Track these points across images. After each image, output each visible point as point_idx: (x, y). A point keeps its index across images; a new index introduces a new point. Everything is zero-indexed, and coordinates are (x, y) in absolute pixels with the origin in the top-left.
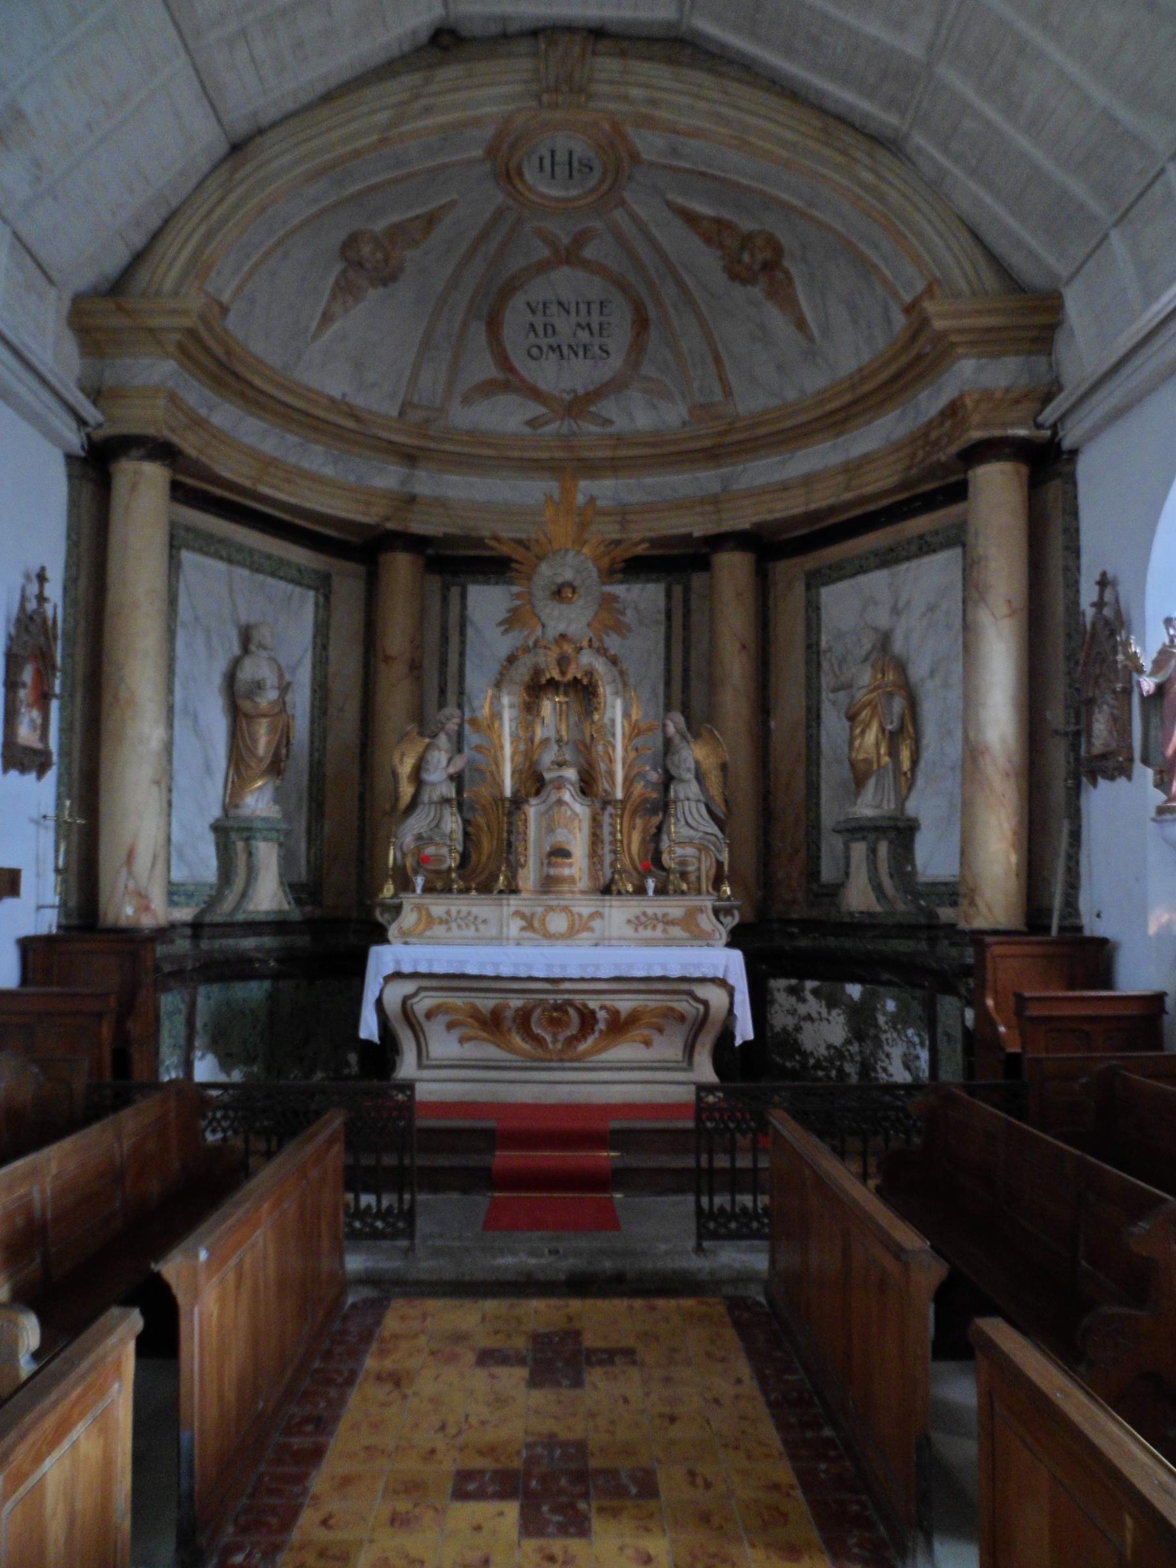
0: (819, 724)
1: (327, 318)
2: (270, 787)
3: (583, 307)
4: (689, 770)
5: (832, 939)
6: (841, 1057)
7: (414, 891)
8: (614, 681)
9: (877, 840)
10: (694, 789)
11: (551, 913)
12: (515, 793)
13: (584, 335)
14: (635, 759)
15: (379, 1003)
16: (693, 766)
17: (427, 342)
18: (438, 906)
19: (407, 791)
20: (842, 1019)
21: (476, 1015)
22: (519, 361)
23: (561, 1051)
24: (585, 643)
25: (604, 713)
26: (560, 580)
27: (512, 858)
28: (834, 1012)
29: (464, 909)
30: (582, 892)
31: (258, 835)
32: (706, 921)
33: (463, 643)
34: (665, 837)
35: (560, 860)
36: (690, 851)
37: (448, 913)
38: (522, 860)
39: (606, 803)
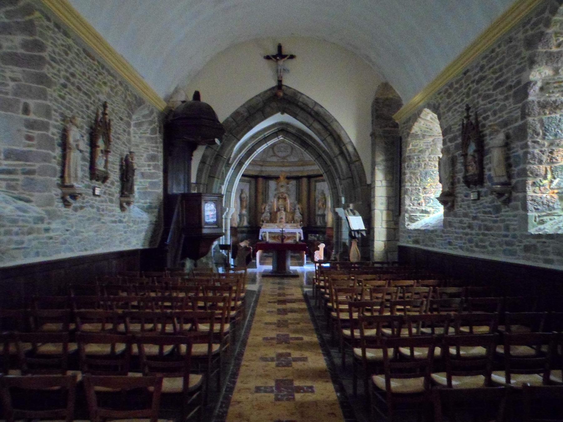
18: (267, 224)
19: (263, 211)
22: (276, 152)
32: (299, 226)
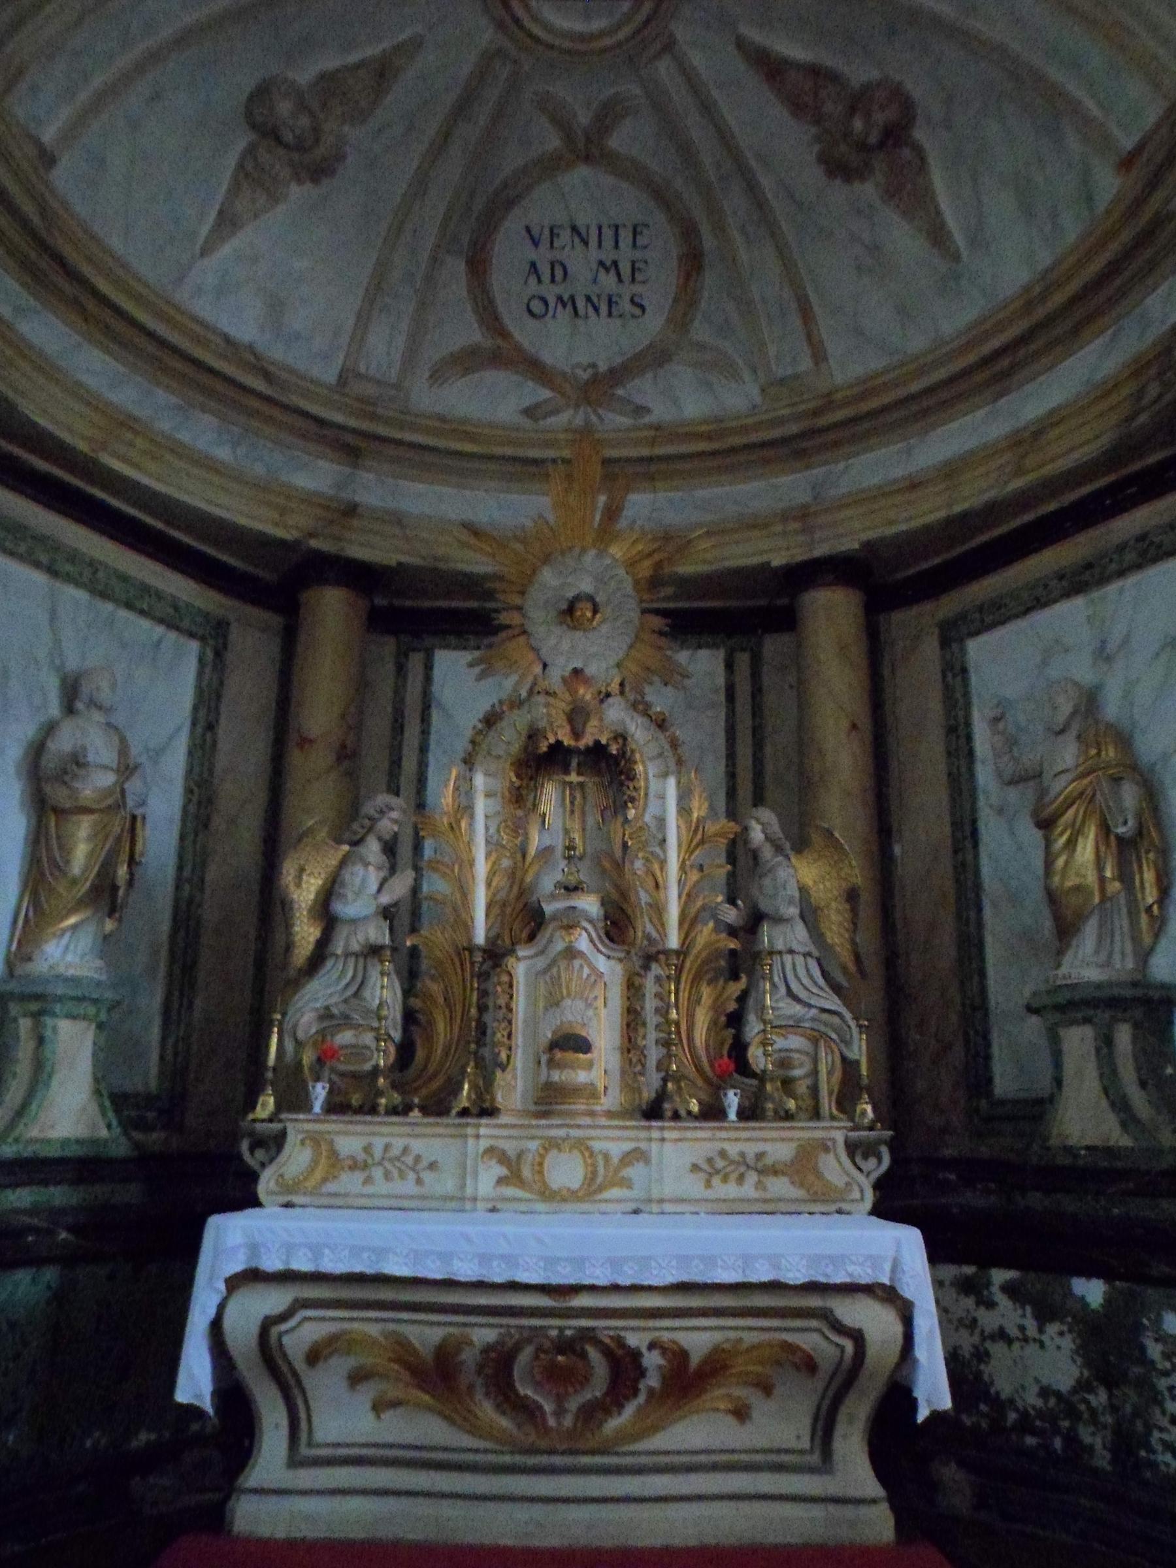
0: (976, 845)
1: (227, 222)
2: (90, 930)
3: (608, 233)
4: (791, 902)
5: (1038, 1195)
6: (1072, 1413)
7: (308, 1108)
8: (660, 755)
9: (1115, 1020)
10: (797, 935)
11: (554, 1152)
12: (492, 940)
13: (608, 281)
14: (698, 882)
15: (216, 1326)
16: (797, 894)
17: (377, 287)
18: (350, 1138)
20: (1068, 1343)
21: (403, 1355)
23: (571, 1434)
24: (614, 687)
25: (646, 805)
26: (570, 594)
27: (486, 1052)
28: (1052, 1329)
29: (398, 1144)
30: (610, 1114)
31: (58, 1008)
32: (835, 1168)
33: (425, 733)
34: (752, 1018)
35: (570, 1056)
36: (795, 1042)
37: (367, 1149)
38: (503, 1056)
39: (649, 959)
